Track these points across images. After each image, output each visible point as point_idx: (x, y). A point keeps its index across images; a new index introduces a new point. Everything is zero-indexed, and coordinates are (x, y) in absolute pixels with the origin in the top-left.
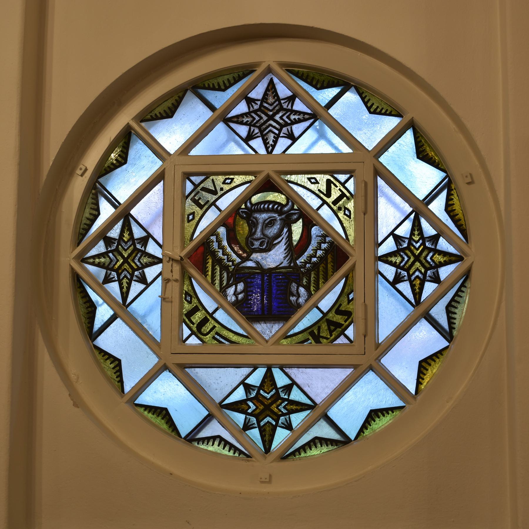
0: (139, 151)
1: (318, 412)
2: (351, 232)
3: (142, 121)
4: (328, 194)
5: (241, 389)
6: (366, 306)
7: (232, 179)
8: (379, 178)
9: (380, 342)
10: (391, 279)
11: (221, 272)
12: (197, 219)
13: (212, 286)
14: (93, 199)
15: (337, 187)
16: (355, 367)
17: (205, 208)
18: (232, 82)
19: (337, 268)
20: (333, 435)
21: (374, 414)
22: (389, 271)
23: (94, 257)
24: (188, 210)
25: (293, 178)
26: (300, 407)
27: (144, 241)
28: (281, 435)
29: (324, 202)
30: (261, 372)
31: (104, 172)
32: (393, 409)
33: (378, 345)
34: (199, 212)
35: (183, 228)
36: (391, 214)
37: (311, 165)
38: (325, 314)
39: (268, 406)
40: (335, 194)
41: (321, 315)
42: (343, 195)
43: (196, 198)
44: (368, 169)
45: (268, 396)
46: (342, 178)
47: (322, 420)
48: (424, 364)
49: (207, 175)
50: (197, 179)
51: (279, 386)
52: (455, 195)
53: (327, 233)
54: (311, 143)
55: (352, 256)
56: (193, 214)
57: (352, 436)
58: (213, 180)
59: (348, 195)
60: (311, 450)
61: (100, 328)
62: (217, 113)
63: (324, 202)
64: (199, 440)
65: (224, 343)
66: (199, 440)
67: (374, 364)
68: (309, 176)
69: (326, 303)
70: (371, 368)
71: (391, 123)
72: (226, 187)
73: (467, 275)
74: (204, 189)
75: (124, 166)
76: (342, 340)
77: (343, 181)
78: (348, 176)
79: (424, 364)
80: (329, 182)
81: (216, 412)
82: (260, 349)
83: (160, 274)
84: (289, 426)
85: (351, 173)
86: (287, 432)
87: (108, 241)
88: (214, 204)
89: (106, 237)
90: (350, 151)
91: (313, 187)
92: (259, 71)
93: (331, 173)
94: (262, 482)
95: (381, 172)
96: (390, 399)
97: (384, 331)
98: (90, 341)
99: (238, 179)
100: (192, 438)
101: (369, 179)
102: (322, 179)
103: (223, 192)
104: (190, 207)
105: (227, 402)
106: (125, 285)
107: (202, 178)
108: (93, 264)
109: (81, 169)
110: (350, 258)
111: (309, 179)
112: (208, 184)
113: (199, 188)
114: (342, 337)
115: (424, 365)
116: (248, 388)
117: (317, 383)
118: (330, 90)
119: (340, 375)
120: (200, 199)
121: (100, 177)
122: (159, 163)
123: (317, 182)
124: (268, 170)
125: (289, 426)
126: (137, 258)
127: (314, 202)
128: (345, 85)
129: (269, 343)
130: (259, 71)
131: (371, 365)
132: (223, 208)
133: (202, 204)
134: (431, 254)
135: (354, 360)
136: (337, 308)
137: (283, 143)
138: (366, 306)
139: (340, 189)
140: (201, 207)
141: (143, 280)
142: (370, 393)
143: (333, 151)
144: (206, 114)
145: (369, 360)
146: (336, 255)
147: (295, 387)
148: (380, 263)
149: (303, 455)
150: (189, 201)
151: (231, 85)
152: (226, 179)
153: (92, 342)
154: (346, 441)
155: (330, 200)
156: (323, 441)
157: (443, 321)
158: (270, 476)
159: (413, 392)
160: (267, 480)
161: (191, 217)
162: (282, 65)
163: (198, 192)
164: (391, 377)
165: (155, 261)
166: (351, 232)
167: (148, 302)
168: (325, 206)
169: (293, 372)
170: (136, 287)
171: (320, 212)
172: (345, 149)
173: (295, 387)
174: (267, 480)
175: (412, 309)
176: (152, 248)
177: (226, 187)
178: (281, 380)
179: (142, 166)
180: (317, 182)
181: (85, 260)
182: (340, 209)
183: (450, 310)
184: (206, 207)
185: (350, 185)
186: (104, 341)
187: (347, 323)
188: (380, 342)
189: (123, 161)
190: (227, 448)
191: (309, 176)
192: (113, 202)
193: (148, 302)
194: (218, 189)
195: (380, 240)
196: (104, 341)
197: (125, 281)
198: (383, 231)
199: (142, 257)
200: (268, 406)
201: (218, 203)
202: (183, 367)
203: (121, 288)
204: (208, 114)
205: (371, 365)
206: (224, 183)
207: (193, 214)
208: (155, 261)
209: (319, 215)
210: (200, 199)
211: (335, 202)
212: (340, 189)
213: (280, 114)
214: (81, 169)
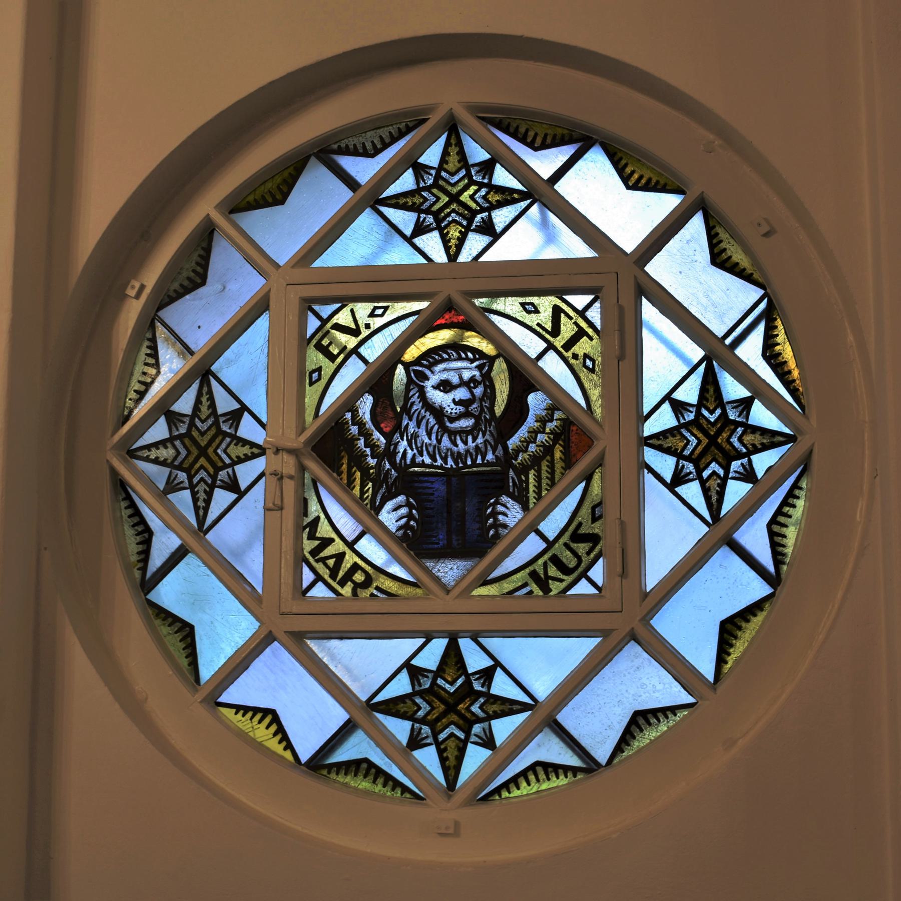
0: (224, 258)
1: (541, 714)
2: (595, 394)
3: (232, 212)
4: (556, 331)
5: (404, 676)
6: (622, 524)
8: (644, 300)
9: (648, 590)
10: (668, 477)
11: (350, 468)
12: (323, 382)
13: (347, 492)
14: (148, 347)
15: (570, 318)
16: (605, 633)
17: (339, 360)
18: (387, 140)
19: (569, 464)
21: (641, 719)
22: (665, 465)
23: (148, 447)
24: (310, 366)
26: (509, 707)
27: (235, 417)
28: (475, 758)
30: (439, 646)
31: (167, 300)
32: (674, 709)
33: (646, 595)
34: (328, 367)
35: (301, 395)
36: (666, 362)
37: (528, 279)
39: (451, 703)
40: (567, 329)
41: (544, 545)
42: (581, 333)
43: (325, 342)
45: (452, 689)
46: (580, 301)
47: (547, 730)
48: (729, 626)
51: (470, 671)
52: (781, 327)
53: (558, 399)
54: (524, 239)
55: (597, 439)
57: (602, 754)
58: (352, 311)
59: (590, 331)
61: (159, 570)
62: (361, 193)
63: (550, 347)
65: (376, 596)
67: (641, 631)
68: (521, 300)
69: (553, 524)
70: (633, 637)
71: (665, 204)
72: (377, 323)
73: (806, 465)
74: (337, 327)
75: (201, 291)
76: (583, 588)
78: (591, 297)
79: (729, 626)
80: (557, 312)
81: (360, 718)
82: (440, 602)
83: (262, 475)
84: (488, 742)
85: (596, 293)
86: (486, 753)
87: (173, 418)
89: (169, 411)
92: (434, 119)
93: (560, 293)
94: (441, 834)
96: (670, 692)
98: (142, 594)
99: (400, 308)
100: (318, 764)
101: (627, 300)
104: (315, 358)
105: (380, 698)
106: (202, 496)
108: (147, 459)
110: (595, 443)
112: (344, 318)
113: (329, 325)
114: (584, 581)
115: (729, 629)
116: (415, 673)
117: (537, 664)
119: (580, 648)
120: (330, 344)
121: (160, 308)
123: (537, 311)
124: (450, 289)
125: (488, 742)
126: (223, 446)
127: (532, 345)
128: (582, 140)
129: (451, 594)
131: (633, 629)
133: (336, 352)
134: (179, 459)
136: (574, 533)
137: (475, 243)
138: (622, 524)
139: (576, 323)
140: (332, 358)
141: (232, 485)
142: (640, 682)
145: (628, 622)
146: (570, 436)
147: (499, 670)
148: (646, 449)
149: (402, 126)
151: (386, 146)
152: (375, 308)
153: (146, 594)
154: (591, 765)
155: (559, 342)
156: (550, 769)
157: (342, 755)
158: (457, 824)
159: (711, 678)
160: (451, 831)
161: (315, 375)
165: (258, 451)
166: (595, 394)
167: (241, 527)
169: (492, 643)
170: (222, 498)
173: (499, 670)
174: (451, 831)
175: (706, 529)
176: (248, 429)
178: (475, 661)
180: (537, 311)
181: (133, 454)
184: (342, 357)
185: (595, 314)
186: (169, 593)
187: (592, 555)
188: (648, 590)
189: (199, 281)
190: (380, 780)
193: (241, 527)
195: (646, 410)
196: (169, 593)
197: (202, 487)
198: (652, 393)
199: (232, 445)
200: (451, 703)
201: (362, 350)
203: (195, 500)
204: (344, 195)
206: (372, 315)
207: (319, 370)
208: (258, 451)
210: (330, 344)
211: (568, 345)
212: (576, 323)
213: (471, 191)
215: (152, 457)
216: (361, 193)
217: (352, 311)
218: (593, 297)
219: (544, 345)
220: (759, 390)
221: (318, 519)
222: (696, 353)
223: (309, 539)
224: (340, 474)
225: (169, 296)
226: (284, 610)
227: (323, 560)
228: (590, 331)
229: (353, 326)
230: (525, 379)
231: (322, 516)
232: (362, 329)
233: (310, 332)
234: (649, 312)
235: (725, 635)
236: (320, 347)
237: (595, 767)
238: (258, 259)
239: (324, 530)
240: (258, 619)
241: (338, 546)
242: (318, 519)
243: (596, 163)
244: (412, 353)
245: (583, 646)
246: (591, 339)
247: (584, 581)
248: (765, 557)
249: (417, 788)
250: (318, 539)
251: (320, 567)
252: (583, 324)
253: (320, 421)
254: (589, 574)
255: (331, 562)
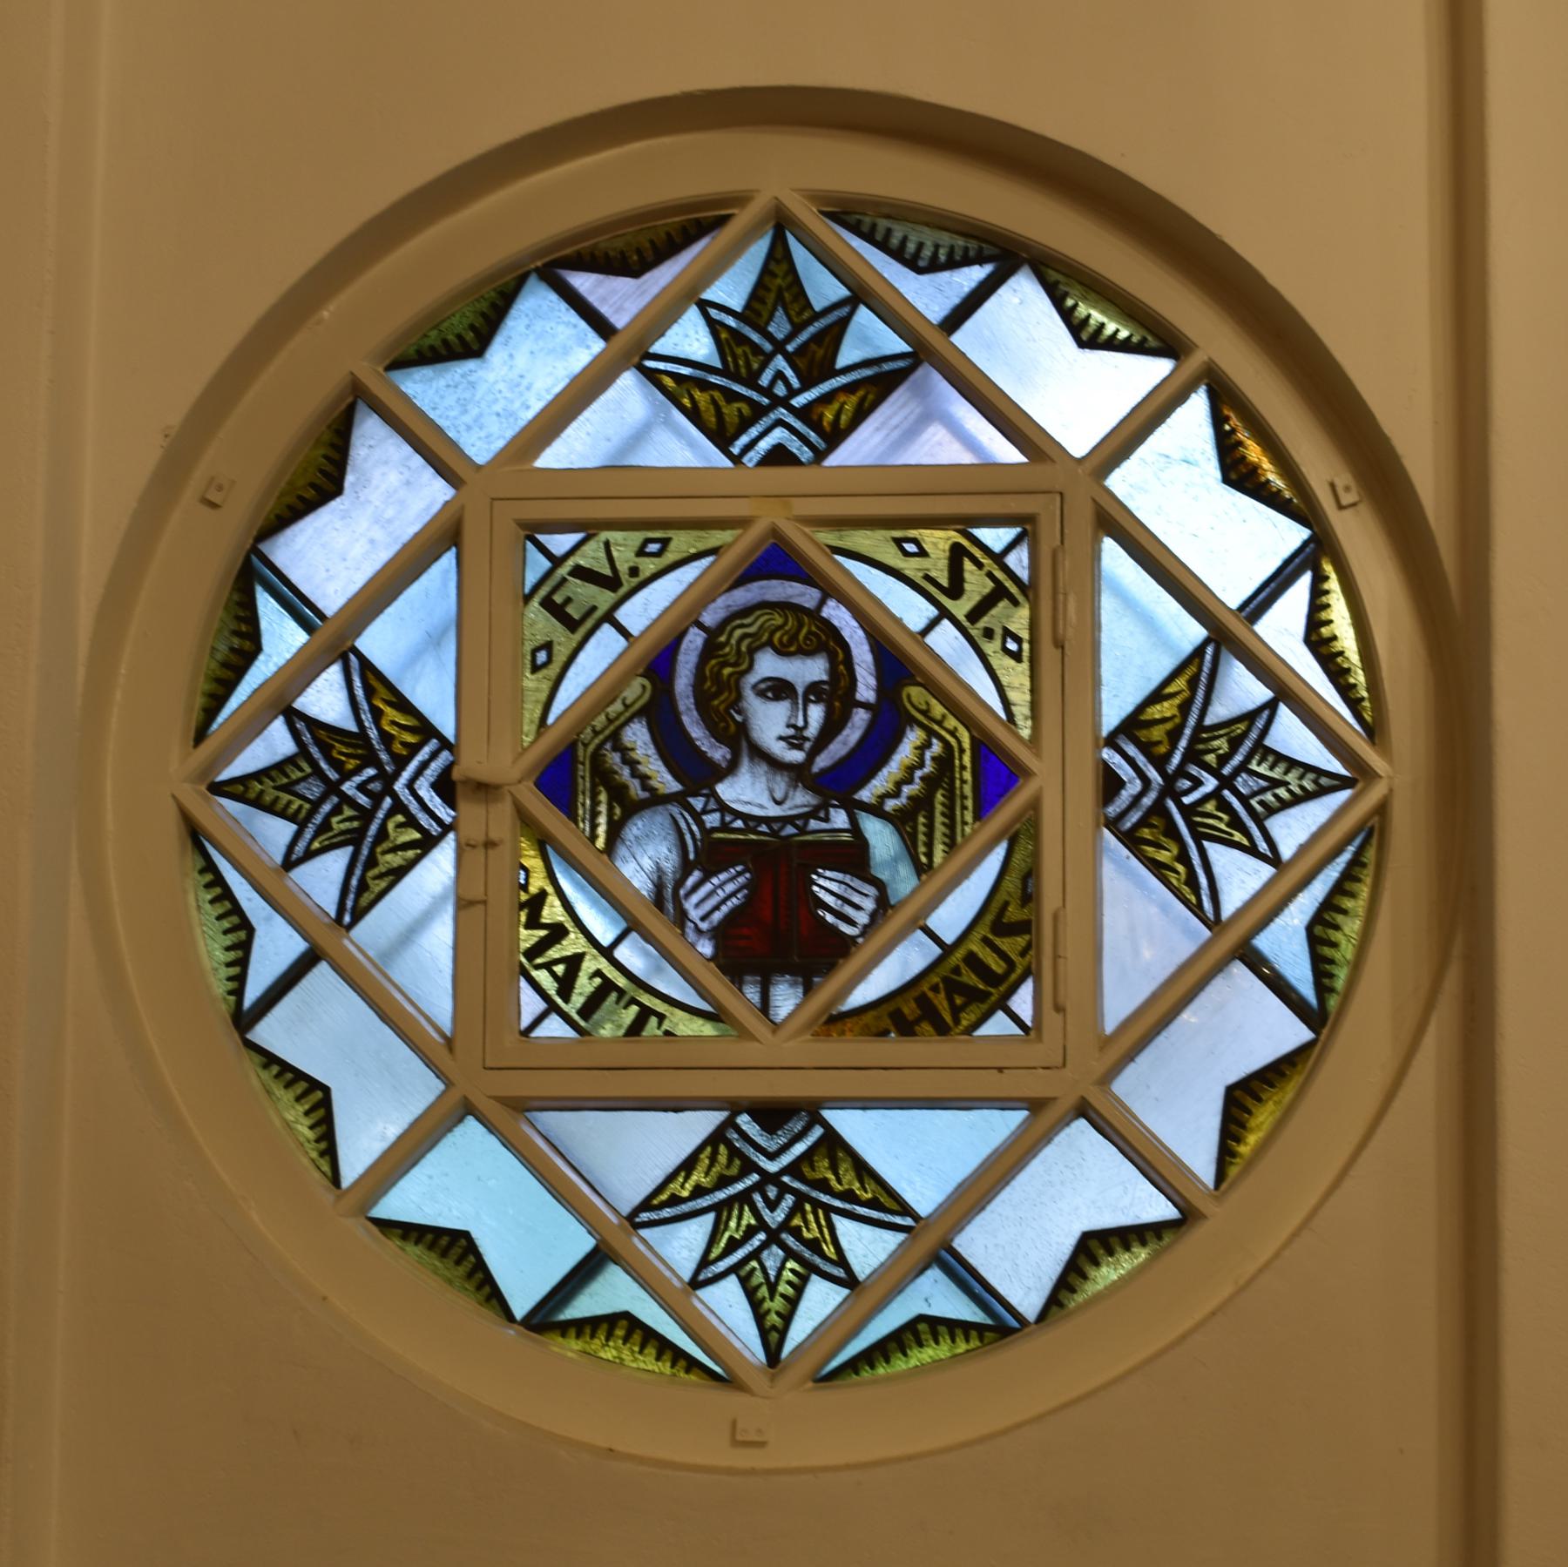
0: (379, 457)
2: (1020, 698)
4: (955, 589)
7: (665, 542)
15: (980, 565)
16: (1035, 1106)
17: (582, 631)
19: (983, 809)
20: (962, 1309)
21: (1094, 1246)
25: (862, 540)
29: (944, 613)
38: (947, 950)
40: (976, 584)
44: (494, 518)
49: (589, 528)
50: (560, 543)
56: (548, 646)
58: (607, 545)
59: (1014, 589)
60: (641, 1352)
63: (944, 613)
64: (564, 1328)
66: (564, 1328)
67: (1097, 1100)
68: (898, 534)
70: (1083, 1110)
74: (580, 573)
76: (998, 1025)
77: (997, 547)
80: (957, 555)
88: (609, 618)
90: (1022, 459)
91: (911, 567)
95: (1117, 523)
97: (1120, 1000)
100: (545, 1319)
102: (938, 541)
103: (635, 581)
107: (575, 538)
109: (1347, 489)
111: (898, 542)
113: (563, 571)
114: (1000, 1015)
115: (1241, 1100)
117: (917, 1151)
118: (966, 270)
120: (568, 600)
122: (437, 492)
123: (922, 553)
127: (911, 609)
130: (743, 219)
132: (635, 628)
133: (576, 616)
135: (1034, 1087)
140: (571, 624)
143: (967, 458)
144: (587, 348)
150: (535, 603)
155: (960, 608)
157: (584, 1306)
162: (817, 197)
163: (564, 580)
164: (1024, 1132)
168: (946, 624)
171: (931, 639)
172: (1009, 453)
177: (649, 566)
179: (390, 495)
182: (988, 633)
183: (1319, 933)
184: (589, 624)
185: (1019, 561)
191: (898, 534)
192: (298, 606)
194: (623, 568)
202: (522, 1106)
205: (465, 1098)
206: (641, 552)
207: (548, 646)
209: (929, 651)
210: (568, 600)
211: (975, 615)
212: (990, 575)
214: (1347, 489)
215: (252, 795)
216: (618, 342)
217: (607, 545)
218: (1019, 530)
219: (932, 612)
220: (1285, 692)
221: (542, 895)
222: (1195, 632)
223: (528, 926)
224: (573, 817)
225: (981, 1338)
226: (489, 1064)
227: (548, 966)
228: (1014, 589)
229: (607, 571)
230: (898, 664)
231: (550, 889)
232: (624, 576)
233: (531, 579)
234: (1113, 555)
235: (1234, 1110)
236: (547, 604)
237: (1014, 1324)
238: (436, 452)
239: (553, 912)
240: (440, 1074)
241: (573, 944)
242: (542, 895)
243: (1023, 297)
244: (710, 618)
245: (1001, 1125)
246: (1015, 603)
247: (1000, 1015)
248: (1300, 974)
249: (717, 1363)
250: (544, 926)
251: (542, 977)
252: (999, 574)
253: (550, 739)
254: (937, 951)
255: (560, 969)
